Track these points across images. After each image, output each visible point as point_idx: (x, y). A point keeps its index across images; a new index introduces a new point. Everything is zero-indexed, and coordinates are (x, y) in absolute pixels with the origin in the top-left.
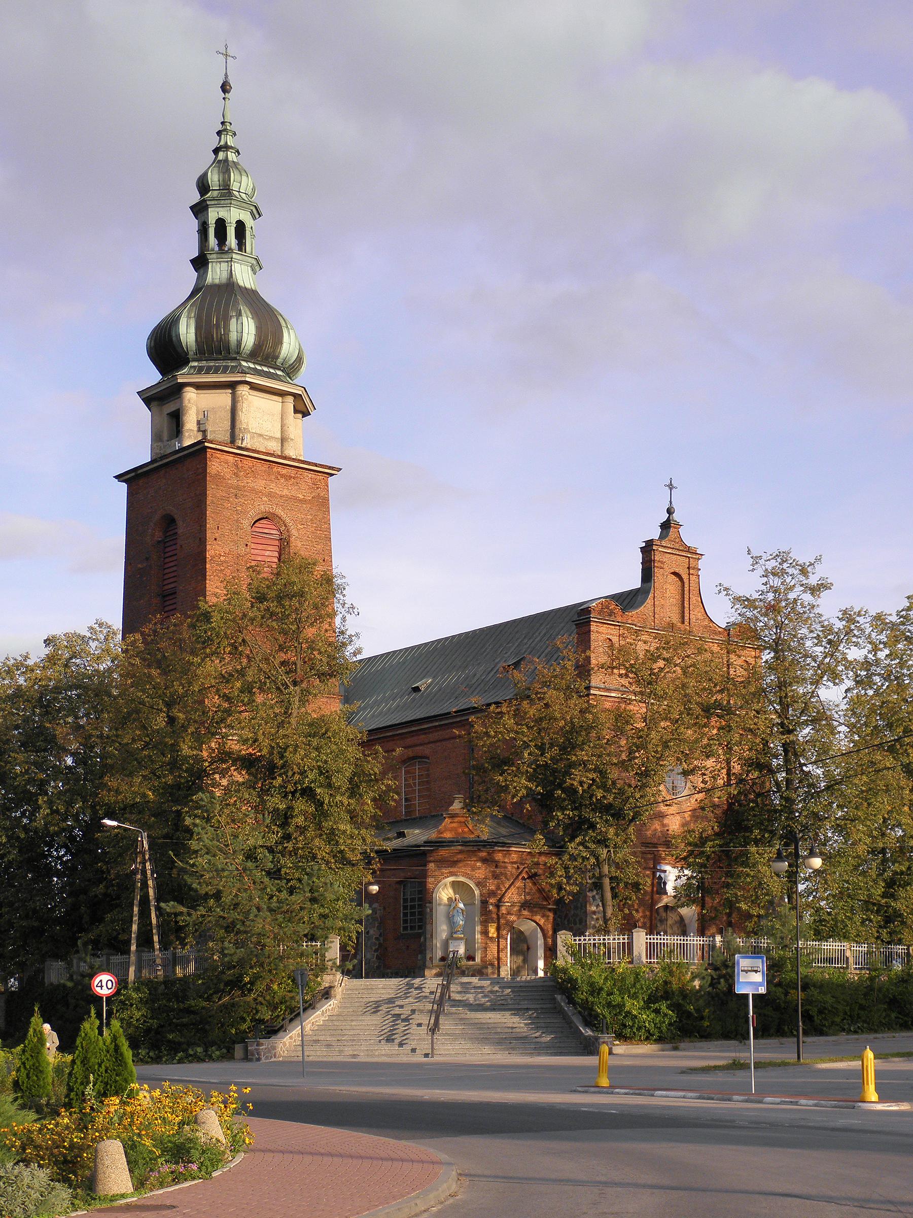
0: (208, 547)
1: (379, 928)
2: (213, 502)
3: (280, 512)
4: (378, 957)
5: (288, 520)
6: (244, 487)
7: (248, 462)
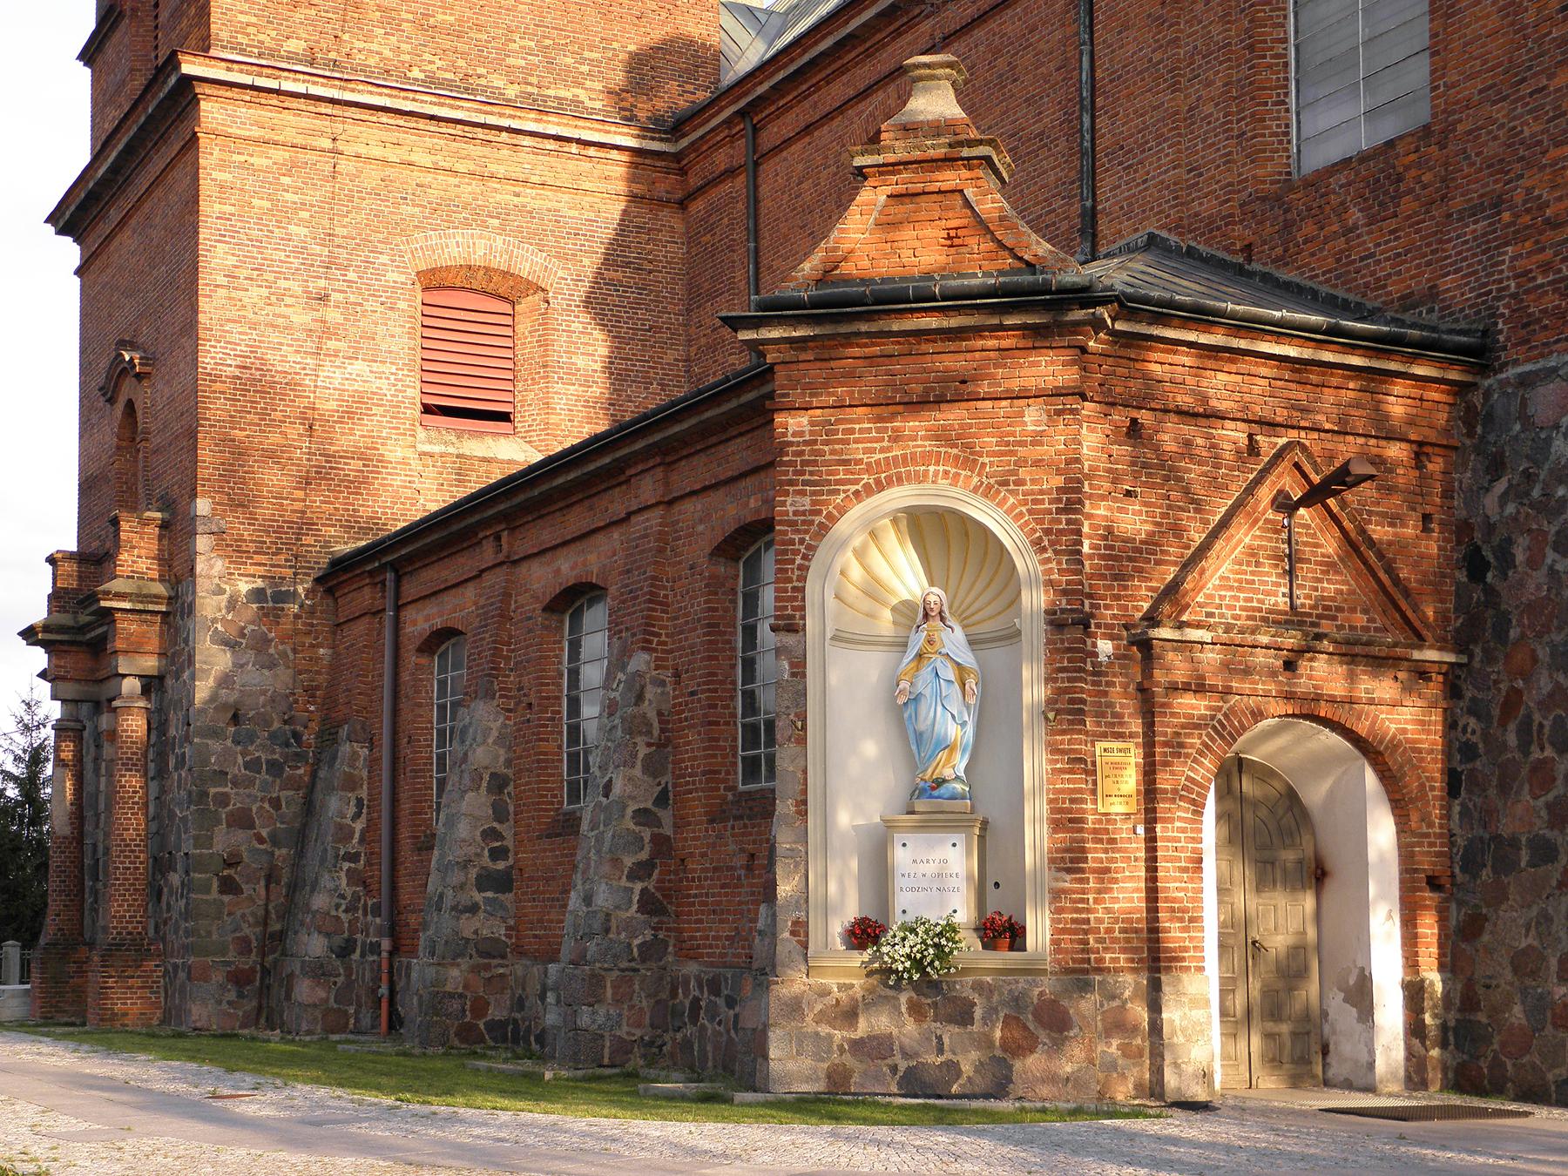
1: (653, 767)
4: (649, 905)
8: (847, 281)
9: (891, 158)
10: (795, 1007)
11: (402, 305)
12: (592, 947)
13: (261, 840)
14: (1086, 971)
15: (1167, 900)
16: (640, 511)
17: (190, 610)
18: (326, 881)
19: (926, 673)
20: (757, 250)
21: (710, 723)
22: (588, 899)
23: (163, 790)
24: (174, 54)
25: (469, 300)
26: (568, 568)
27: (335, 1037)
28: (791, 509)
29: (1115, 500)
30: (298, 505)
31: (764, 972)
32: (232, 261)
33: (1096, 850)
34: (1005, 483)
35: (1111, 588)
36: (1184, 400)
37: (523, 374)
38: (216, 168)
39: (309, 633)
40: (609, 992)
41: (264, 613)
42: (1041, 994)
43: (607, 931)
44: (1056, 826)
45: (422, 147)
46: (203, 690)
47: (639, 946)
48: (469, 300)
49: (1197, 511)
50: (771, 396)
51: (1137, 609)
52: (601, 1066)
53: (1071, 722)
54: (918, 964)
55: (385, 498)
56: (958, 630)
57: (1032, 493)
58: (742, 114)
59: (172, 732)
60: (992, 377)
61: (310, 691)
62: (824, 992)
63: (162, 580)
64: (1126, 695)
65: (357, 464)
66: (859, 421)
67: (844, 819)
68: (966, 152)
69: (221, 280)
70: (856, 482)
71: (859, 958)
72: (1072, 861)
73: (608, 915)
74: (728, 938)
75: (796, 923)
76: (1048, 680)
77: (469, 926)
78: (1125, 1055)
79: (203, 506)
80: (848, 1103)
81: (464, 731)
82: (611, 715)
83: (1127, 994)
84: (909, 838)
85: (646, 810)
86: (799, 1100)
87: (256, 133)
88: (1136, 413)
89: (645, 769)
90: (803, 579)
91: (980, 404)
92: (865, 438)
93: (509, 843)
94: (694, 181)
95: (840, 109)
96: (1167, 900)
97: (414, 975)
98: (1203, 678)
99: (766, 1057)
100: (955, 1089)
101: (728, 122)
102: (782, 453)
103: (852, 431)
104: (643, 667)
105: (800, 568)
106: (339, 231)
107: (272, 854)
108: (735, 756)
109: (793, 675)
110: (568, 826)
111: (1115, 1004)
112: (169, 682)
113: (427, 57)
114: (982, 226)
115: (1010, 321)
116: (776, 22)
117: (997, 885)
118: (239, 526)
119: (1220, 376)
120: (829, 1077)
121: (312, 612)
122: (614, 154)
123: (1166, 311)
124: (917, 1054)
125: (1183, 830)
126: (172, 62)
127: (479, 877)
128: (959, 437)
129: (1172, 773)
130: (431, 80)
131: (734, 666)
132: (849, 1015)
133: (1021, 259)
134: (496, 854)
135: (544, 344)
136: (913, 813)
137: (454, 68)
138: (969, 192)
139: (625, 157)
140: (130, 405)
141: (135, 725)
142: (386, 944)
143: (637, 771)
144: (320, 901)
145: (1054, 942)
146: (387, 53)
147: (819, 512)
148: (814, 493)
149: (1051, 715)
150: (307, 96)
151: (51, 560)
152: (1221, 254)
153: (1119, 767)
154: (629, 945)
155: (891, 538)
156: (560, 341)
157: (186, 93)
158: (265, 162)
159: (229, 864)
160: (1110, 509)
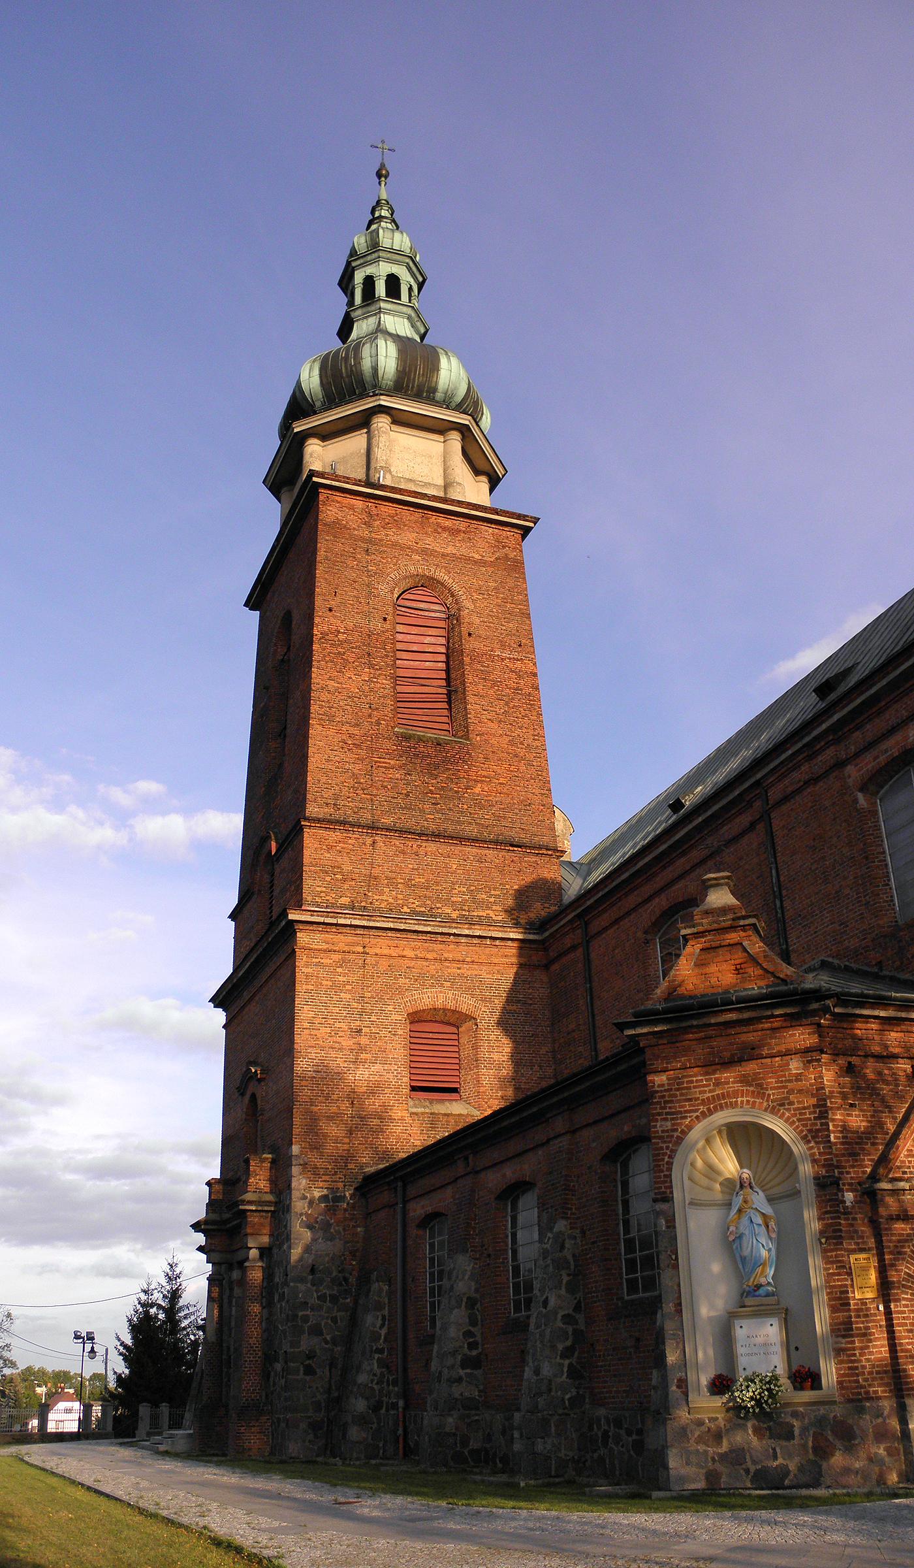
0: (317, 620)
1: (572, 1288)
2: (327, 558)
3: (441, 575)
4: (573, 1373)
5: (455, 587)
6: (381, 540)
7: (387, 509)
8: (682, 997)
9: (701, 929)
10: (683, 1432)
11: (400, 1032)
12: (541, 1401)
13: (327, 1342)
14: (860, 1401)
15: (902, 1351)
16: (556, 1137)
17: (288, 1209)
18: (365, 1366)
19: (745, 1220)
20: (591, 988)
21: (606, 1260)
22: (537, 1372)
23: (271, 1314)
24: (285, 910)
25: (435, 1026)
26: (510, 1173)
27: (373, 1462)
28: (660, 1129)
29: (845, 1109)
30: (346, 1147)
31: (662, 1413)
32: (312, 1014)
33: (857, 1323)
34: (782, 1105)
35: (848, 1161)
36: (876, 1049)
37: (464, 1063)
38: (304, 966)
39: (351, 1219)
40: (553, 1429)
41: (328, 1209)
42: (835, 1417)
43: (550, 1390)
44: (834, 1309)
45: (409, 948)
46: (296, 1253)
47: (569, 1399)
48: (435, 1026)
49: (890, 1112)
50: (644, 1063)
51: (865, 1172)
52: (551, 1476)
53: (836, 1244)
54: (759, 1403)
55: (393, 1140)
56: (760, 1193)
57: (798, 1109)
58: (578, 916)
59: (277, 1280)
60: (769, 1044)
61: (353, 1254)
62: (700, 1423)
63: (271, 1192)
64: (863, 1225)
65: (376, 1121)
66: (695, 1075)
67: (704, 1311)
68: (742, 923)
69: (306, 1025)
70: (696, 1111)
71: (718, 1401)
72: (845, 1330)
73: (550, 1381)
74: (624, 1391)
75: (680, 1380)
76: (820, 1219)
77: (457, 1391)
78: (889, 1454)
79: (295, 1149)
80: (724, 1495)
81: (450, 1273)
82: (544, 1258)
83: (886, 1413)
84: (745, 1323)
85: (568, 1315)
86: (693, 1495)
87: (325, 946)
88: (851, 1057)
89: (568, 1291)
90: (670, 1169)
91: (763, 1061)
92: (702, 1084)
93: (479, 1338)
94: (553, 954)
95: (634, 909)
96: (902, 1351)
97: (425, 1422)
98: (906, 1211)
99: (666, 1467)
100: (787, 1482)
101: (570, 921)
102: (653, 1097)
103: (692, 1082)
104: (563, 1229)
105: (668, 1163)
106: (368, 995)
107: (333, 1350)
108: (621, 1278)
109: (668, 1227)
110: (519, 1327)
111: (880, 1420)
112: (275, 1251)
113: (411, 900)
114: (753, 959)
115: (777, 1012)
116: (585, 868)
117: (797, 1349)
118: (314, 1158)
119: (892, 1034)
120: (707, 1479)
121: (353, 1207)
122: (510, 943)
123: (863, 1001)
124: (761, 1461)
125: (906, 1306)
126: (284, 914)
127: (462, 1360)
128: (753, 1080)
129: (896, 1270)
130: (414, 912)
131: (618, 1224)
132: (718, 1437)
133: (779, 978)
134: (472, 1346)
135: (476, 1047)
136: (744, 1307)
137: (425, 905)
138: (745, 943)
139: (515, 944)
140: (253, 1096)
141: (256, 1275)
142: (401, 1403)
143: (563, 1292)
144: (362, 1378)
145: (840, 1383)
146: (391, 900)
147: (676, 1130)
148: (673, 1119)
149: (823, 1240)
150: (351, 926)
151: (209, 1184)
152: (865, 968)
153: (865, 1269)
154: (563, 1399)
155: (718, 1141)
156: (484, 1047)
157: (290, 929)
158: (329, 961)
159: (309, 1357)
160: (841, 1115)
